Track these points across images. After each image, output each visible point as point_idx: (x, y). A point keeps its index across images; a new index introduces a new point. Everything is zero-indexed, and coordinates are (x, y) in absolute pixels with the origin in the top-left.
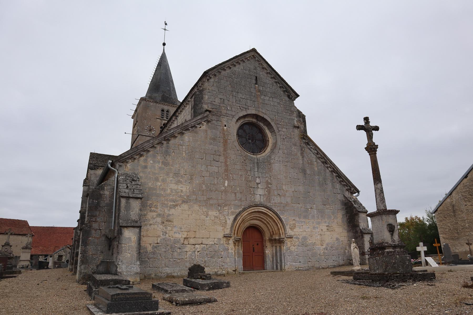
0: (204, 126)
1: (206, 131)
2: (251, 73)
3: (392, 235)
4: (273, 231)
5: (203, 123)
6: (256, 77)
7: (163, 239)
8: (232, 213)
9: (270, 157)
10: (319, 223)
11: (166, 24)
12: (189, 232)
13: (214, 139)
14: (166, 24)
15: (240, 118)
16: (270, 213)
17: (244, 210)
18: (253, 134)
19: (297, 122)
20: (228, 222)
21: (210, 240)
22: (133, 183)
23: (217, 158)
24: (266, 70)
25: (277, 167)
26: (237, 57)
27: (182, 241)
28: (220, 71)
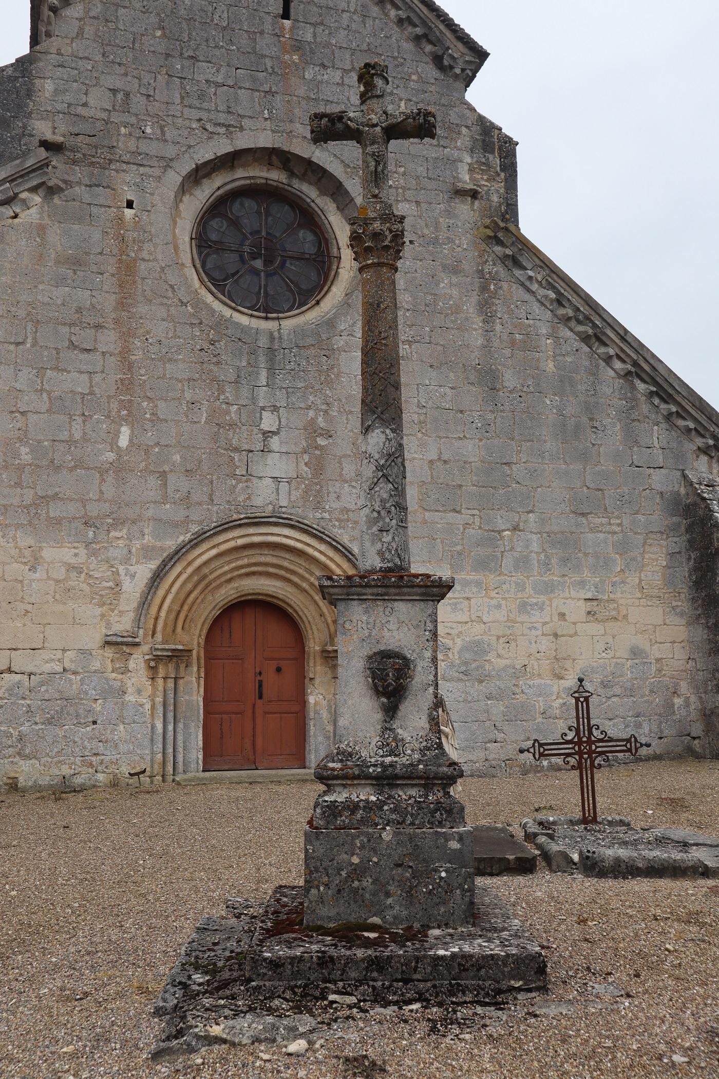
3: (391, 711)
5: (24, 195)
6: (260, 683)
8: (147, 552)
10: (548, 589)
13: (76, 263)
15: (199, 174)
19: (471, 171)
20: (127, 585)
21: (44, 655)
23: (85, 337)
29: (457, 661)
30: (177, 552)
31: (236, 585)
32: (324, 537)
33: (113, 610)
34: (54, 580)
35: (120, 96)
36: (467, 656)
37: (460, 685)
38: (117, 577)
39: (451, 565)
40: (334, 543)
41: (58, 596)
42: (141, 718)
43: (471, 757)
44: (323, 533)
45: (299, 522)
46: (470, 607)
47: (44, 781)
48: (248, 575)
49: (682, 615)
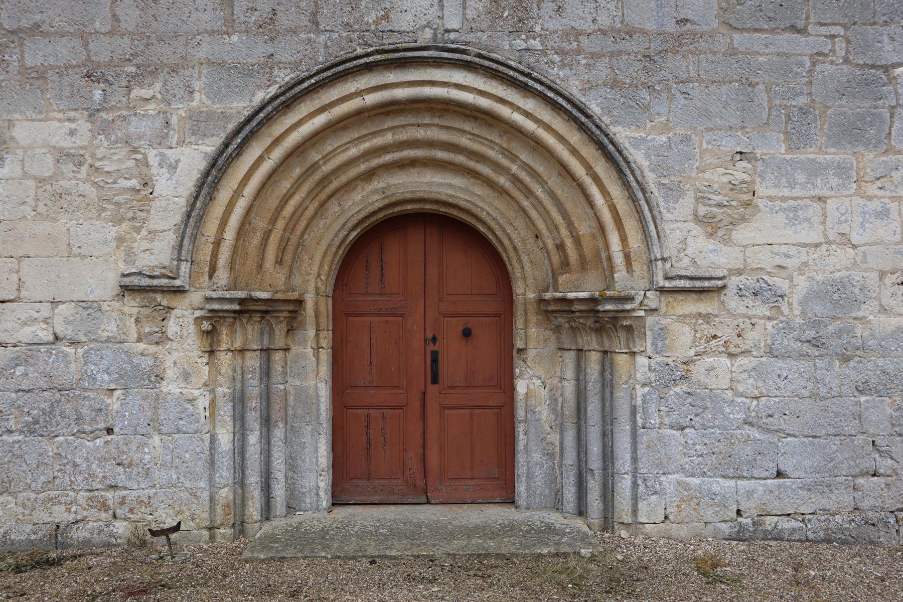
4: (561, 247)
8: (198, 123)
16: (521, 110)
20: (163, 184)
21: (21, 311)
29: (798, 320)
31: (381, 185)
32: (531, 82)
33: (138, 230)
34: (35, 178)
36: (818, 309)
37: (804, 366)
38: (144, 170)
39: (786, 133)
40: (551, 94)
41: (41, 208)
43: (824, 503)
44: (528, 75)
45: (480, 56)
46: (825, 215)
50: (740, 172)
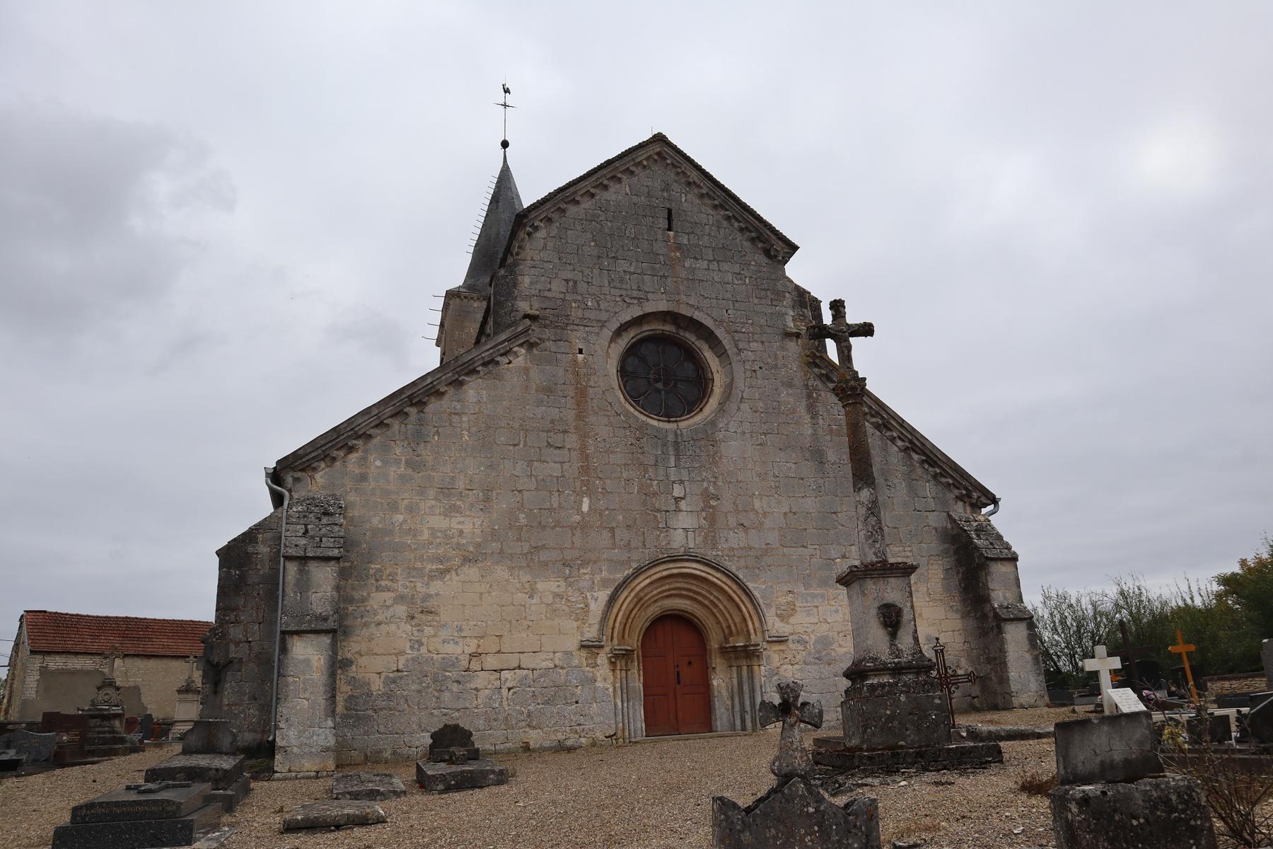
0: (521, 358)
1: (526, 370)
2: (655, 202)
3: (893, 635)
4: (729, 627)
5: (515, 349)
6: (670, 211)
7: (413, 659)
8: (605, 583)
9: (713, 423)
11: (507, 91)
12: (482, 637)
13: (549, 390)
14: (507, 91)
15: (619, 333)
16: (716, 577)
17: (638, 572)
18: (667, 368)
19: (794, 320)
20: (593, 606)
21: (542, 656)
22: (325, 520)
23: (557, 439)
24: (699, 187)
25: (736, 448)
26: (609, 163)
27: (465, 663)
28: (563, 206)
30: (624, 582)
35: (571, 283)
37: (816, 667)
42: (608, 697)
47: (547, 744)
48: (667, 597)
49: (957, 611)
50: (790, 598)
